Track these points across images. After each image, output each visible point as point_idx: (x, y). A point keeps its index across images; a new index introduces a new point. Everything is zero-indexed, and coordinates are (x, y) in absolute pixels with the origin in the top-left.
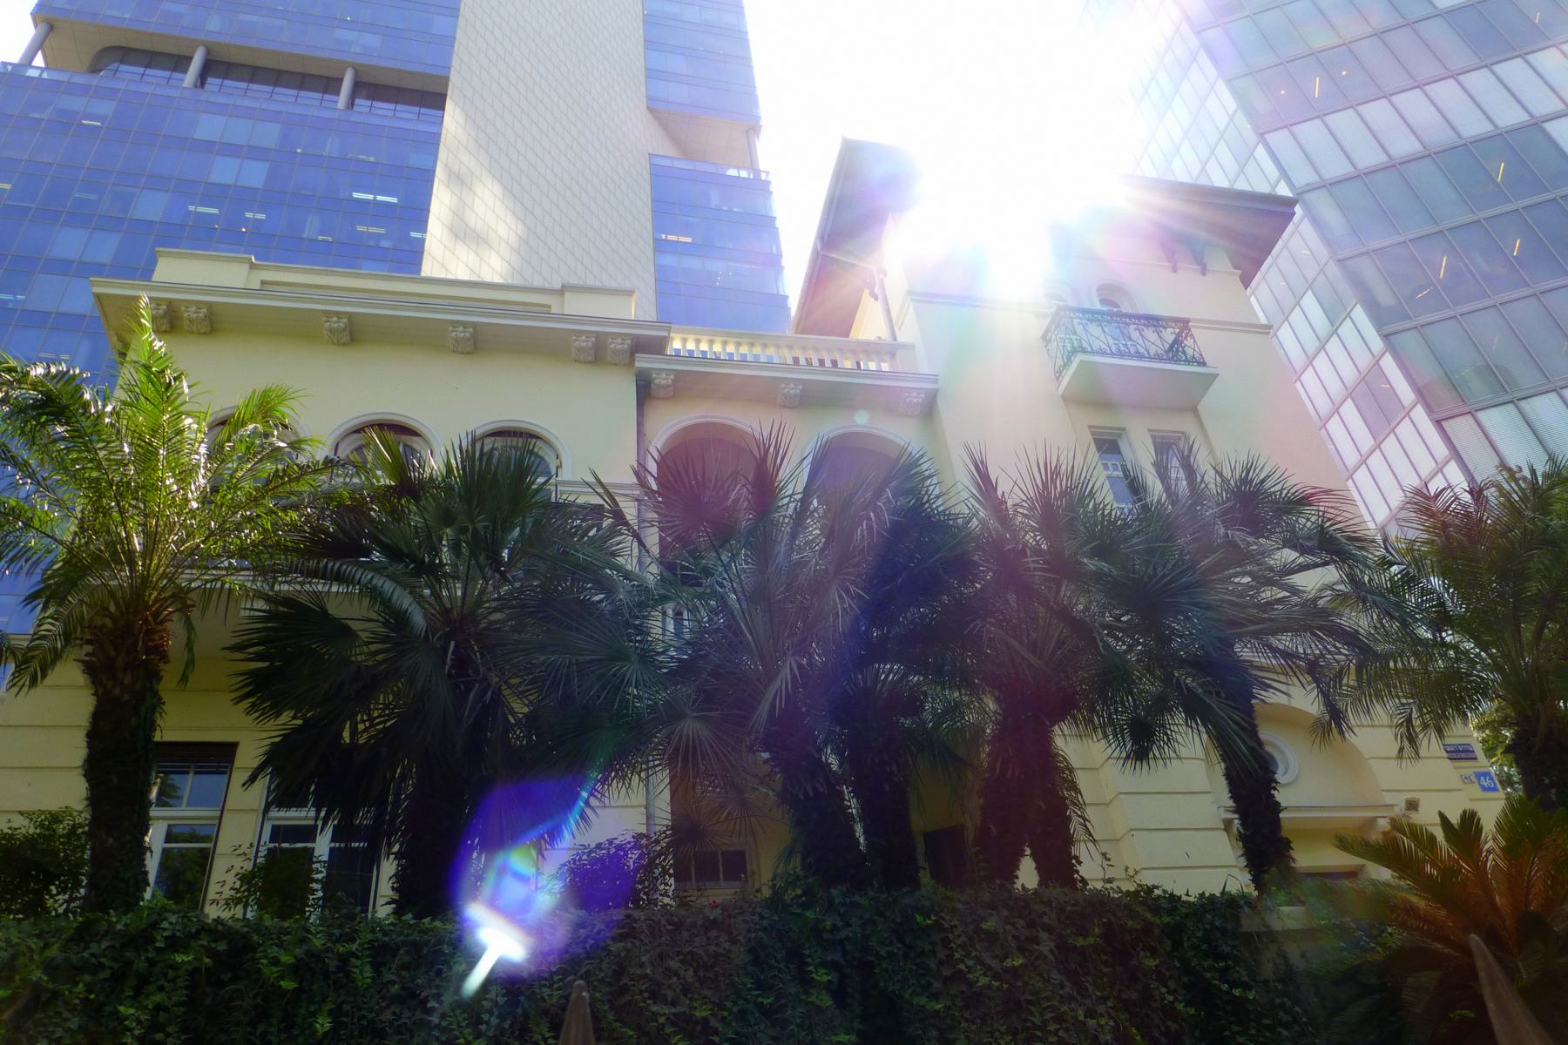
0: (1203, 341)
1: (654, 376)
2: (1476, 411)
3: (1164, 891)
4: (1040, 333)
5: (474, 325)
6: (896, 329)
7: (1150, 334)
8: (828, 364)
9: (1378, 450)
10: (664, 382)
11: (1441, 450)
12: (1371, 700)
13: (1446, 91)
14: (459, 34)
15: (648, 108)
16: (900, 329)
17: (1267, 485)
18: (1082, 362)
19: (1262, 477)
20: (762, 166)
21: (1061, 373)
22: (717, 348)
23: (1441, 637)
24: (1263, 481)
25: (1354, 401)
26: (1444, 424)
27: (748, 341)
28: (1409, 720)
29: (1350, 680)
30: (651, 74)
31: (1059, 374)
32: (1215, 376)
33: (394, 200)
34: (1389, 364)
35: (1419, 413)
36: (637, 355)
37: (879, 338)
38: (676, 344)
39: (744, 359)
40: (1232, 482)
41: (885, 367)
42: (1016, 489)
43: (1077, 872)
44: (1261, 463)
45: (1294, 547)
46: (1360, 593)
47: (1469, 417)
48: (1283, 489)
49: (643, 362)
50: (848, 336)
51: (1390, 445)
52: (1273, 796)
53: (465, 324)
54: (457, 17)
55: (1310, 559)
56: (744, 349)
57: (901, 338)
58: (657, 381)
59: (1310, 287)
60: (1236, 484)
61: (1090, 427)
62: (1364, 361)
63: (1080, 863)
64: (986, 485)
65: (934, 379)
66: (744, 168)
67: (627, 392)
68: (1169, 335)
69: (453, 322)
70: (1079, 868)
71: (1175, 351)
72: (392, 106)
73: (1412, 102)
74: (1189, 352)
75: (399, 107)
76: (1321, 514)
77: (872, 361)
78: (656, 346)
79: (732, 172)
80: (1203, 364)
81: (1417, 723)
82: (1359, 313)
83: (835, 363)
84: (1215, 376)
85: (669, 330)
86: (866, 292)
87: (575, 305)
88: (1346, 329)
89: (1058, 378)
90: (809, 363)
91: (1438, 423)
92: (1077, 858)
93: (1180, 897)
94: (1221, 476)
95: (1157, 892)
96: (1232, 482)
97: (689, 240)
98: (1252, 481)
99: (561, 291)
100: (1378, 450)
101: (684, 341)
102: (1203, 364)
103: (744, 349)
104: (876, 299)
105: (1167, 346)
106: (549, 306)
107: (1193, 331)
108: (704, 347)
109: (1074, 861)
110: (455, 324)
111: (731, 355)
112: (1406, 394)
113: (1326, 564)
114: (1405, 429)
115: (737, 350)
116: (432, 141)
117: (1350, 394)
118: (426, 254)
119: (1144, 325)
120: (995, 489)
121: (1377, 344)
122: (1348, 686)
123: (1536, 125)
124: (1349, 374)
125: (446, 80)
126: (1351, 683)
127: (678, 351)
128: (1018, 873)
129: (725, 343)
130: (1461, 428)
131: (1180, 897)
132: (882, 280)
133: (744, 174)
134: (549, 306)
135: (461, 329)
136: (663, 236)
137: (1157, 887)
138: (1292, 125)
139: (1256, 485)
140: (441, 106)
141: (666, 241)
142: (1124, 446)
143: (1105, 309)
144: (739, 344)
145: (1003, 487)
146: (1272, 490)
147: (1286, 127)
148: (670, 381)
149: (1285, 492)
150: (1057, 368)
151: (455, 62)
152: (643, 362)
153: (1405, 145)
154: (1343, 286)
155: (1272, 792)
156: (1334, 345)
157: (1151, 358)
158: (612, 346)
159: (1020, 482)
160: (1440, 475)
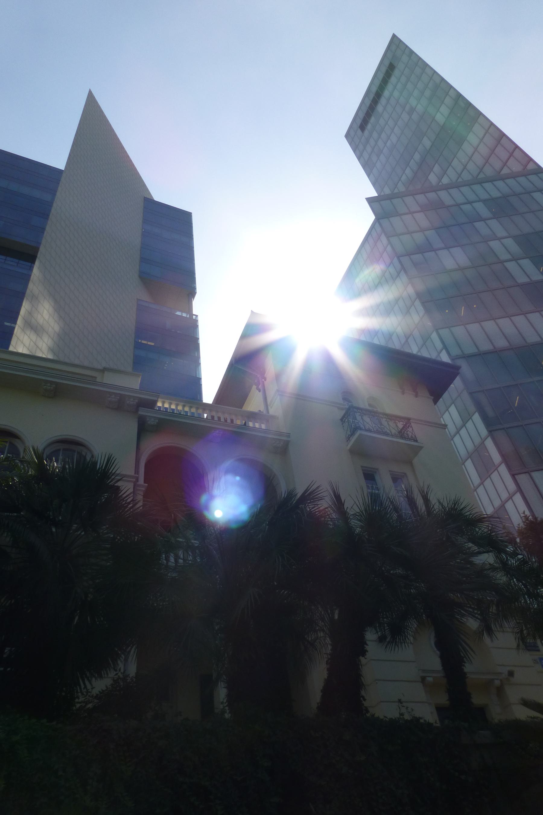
0: (417, 430)
1: (148, 419)
2: (531, 472)
3: (425, 721)
4: (340, 418)
5: (56, 383)
6: (269, 407)
7: (392, 424)
8: (216, 419)
9: (482, 485)
11: (512, 486)
12: (502, 619)
13: (520, 320)
14: (48, 228)
15: (139, 276)
16: (271, 408)
17: (463, 512)
18: (360, 435)
19: (461, 508)
20: (194, 312)
21: (349, 438)
22: (180, 408)
23: (537, 592)
24: (463, 509)
25: (472, 460)
26: (516, 477)
27: (182, 404)
28: (522, 631)
29: (493, 609)
31: (348, 439)
32: (421, 448)
34: (489, 443)
35: (503, 469)
36: (140, 408)
37: (260, 411)
38: (159, 404)
39: (193, 415)
40: (447, 509)
41: (263, 427)
43: (363, 704)
44: (461, 500)
45: (473, 543)
46: (505, 567)
47: (527, 474)
48: (470, 514)
49: (143, 412)
50: (242, 409)
51: (488, 483)
52: (365, 647)
53: (51, 383)
55: (482, 549)
56: (193, 410)
57: (272, 412)
59: (453, 403)
60: (449, 509)
61: (362, 467)
62: (477, 441)
63: (365, 700)
65: (288, 435)
66: (185, 312)
67: (133, 427)
68: (400, 425)
70: (363, 702)
71: (401, 434)
73: (505, 323)
74: (410, 434)
75: (8, 258)
76: (490, 528)
77: (257, 422)
79: (178, 313)
80: (416, 441)
81: (525, 632)
82: (477, 417)
83: (232, 421)
84: (421, 448)
85: (158, 397)
86: (254, 387)
88: (469, 425)
89: (348, 440)
90: (226, 421)
91: (513, 476)
92: (363, 697)
93: (433, 724)
94: (442, 505)
95: (422, 721)
96: (447, 509)
97: (152, 344)
98: (457, 509)
99: (103, 371)
100: (482, 485)
101: (163, 403)
102: (416, 441)
103: (193, 410)
104: (260, 391)
105: (399, 430)
106: (96, 378)
107: (412, 424)
108: (173, 407)
109: (362, 699)
110: (46, 382)
111: (187, 412)
112: (496, 457)
113: (488, 552)
114: (495, 476)
115: (190, 410)
116: (26, 279)
117: (470, 456)
118: (14, 335)
119: (389, 419)
121: (484, 432)
122: (492, 612)
123: (447, 248)
124: (470, 446)
126: (494, 611)
127: (160, 407)
128: (104, 688)
130: (523, 479)
131: (433, 724)
132: (263, 382)
133: (184, 315)
134: (96, 378)
135: (49, 385)
136: (140, 341)
137: (421, 718)
138: (451, 327)
139: (458, 511)
140: (33, 262)
141: (141, 343)
142: (377, 478)
143: (370, 409)
144: (191, 407)
145: (348, 505)
146: (467, 514)
147: (448, 327)
148: (155, 423)
149: (471, 516)
150: (347, 436)
151: (43, 242)
152: (143, 412)
153: (501, 343)
154: (472, 408)
155: (463, 667)
156: (463, 432)
157: (392, 435)
158: (128, 402)
160: (482, 485)
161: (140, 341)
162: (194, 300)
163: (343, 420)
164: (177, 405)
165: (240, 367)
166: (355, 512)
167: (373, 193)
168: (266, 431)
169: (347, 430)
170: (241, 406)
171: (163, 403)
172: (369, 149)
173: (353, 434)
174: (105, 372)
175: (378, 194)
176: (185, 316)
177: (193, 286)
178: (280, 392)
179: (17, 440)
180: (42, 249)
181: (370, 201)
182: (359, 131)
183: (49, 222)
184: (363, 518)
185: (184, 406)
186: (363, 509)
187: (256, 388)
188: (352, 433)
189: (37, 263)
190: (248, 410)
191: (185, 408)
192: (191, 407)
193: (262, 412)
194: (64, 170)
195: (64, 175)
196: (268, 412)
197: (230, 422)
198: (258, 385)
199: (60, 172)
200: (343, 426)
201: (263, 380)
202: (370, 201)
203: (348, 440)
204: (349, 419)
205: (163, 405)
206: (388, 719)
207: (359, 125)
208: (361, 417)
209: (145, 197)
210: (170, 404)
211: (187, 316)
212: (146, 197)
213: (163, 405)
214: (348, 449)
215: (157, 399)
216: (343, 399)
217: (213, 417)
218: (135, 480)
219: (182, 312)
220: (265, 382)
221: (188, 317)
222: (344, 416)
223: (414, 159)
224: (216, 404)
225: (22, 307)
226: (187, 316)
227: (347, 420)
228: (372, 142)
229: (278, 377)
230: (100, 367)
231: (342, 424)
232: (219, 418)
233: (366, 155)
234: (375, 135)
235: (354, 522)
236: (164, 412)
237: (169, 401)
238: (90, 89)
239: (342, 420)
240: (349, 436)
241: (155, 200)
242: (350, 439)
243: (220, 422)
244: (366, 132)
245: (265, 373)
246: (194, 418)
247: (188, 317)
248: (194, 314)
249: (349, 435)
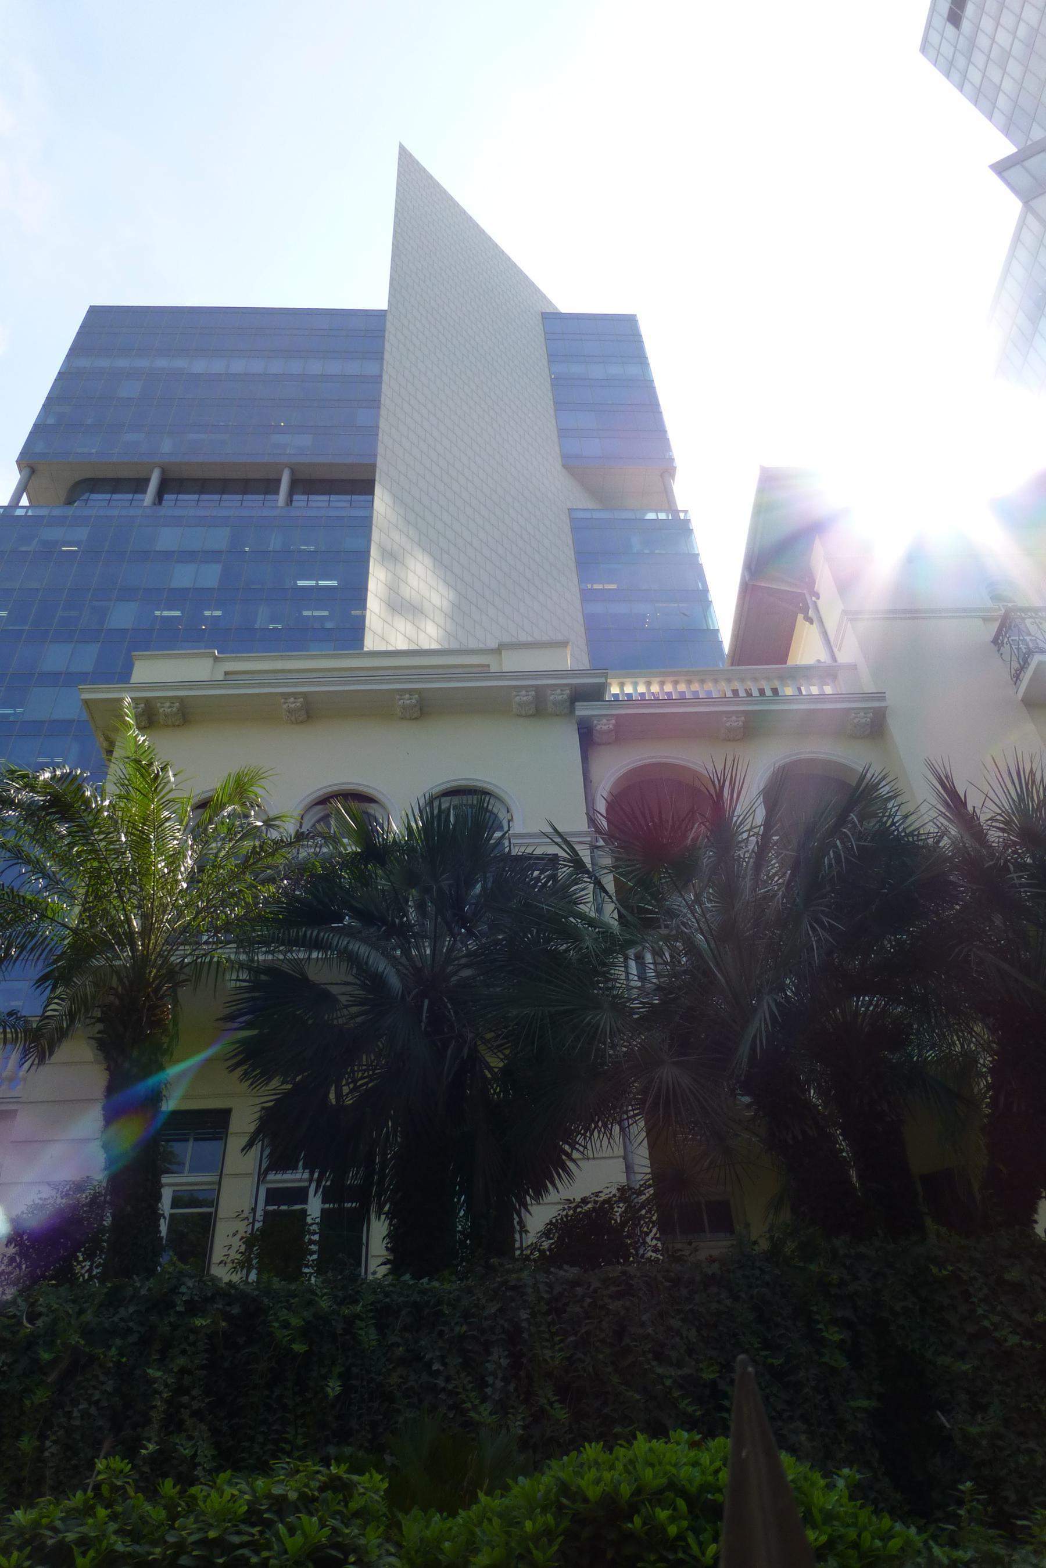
1: (595, 722)
6: (835, 650)
10: (605, 728)
14: (382, 424)
15: (563, 466)
16: (839, 650)
20: (680, 506)
22: (655, 688)
27: (658, 679)
30: (563, 433)
33: (335, 583)
36: (577, 704)
37: (819, 661)
38: (615, 690)
42: (989, 803)
53: (411, 692)
54: (379, 408)
58: (598, 727)
64: (955, 802)
65: (880, 696)
66: (661, 511)
69: (398, 691)
72: (326, 498)
75: (333, 497)
78: (595, 693)
79: (651, 516)
83: (775, 691)
87: (513, 662)
97: (614, 586)
99: (498, 651)
101: (622, 685)
104: (811, 622)
111: (669, 694)
115: (675, 688)
116: (365, 525)
120: (965, 804)
125: (373, 467)
129: (662, 684)
132: (815, 603)
133: (662, 516)
134: (488, 666)
136: (589, 586)
144: (676, 683)
145: (973, 802)
150: (1013, 672)
151: (381, 449)
152: (583, 710)
158: (552, 697)
159: (992, 795)
161: (589, 586)
162: (676, 479)
163: (999, 641)
164: (648, 684)
165: (763, 585)
166: (994, 815)
167: (1007, 148)
168: (838, 697)
169: (1011, 661)
170: (783, 659)
171: (622, 685)
172: (979, 59)
173: (1023, 668)
174: (504, 652)
175: (1017, 148)
176: (665, 518)
177: (667, 457)
178: (851, 616)
179: (373, 805)
180: (380, 463)
181: (1001, 168)
182: (950, 28)
183: (383, 412)
184: (1016, 825)
185: (662, 684)
186: (1007, 808)
187: (804, 618)
188: (1022, 663)
189: (378, 490)
190: (798, 663)
191: (625, 689)
192: (676, 683)
193: (825, 662)
194: (386, 309)
195: (389, 317)
196: (835, 659)
197: (758, 695)
198: (805, 610)
199: (379, 316)
200: (1001, 654)
201: (814, 598)
202: (1001, 168)
203: (1017, 680)
204: (1010, 637)
205: (622, 689)
206: (649, 1174)
207: (946, 15)
208: (1037, 625)
209: (542, 313)
210: (648, 684)
211: (668, 516)
212: (544, 311)
213: (622, 689)
214: (1020, 699)
215: (603, 680)
216: (992, 598)
217: (735, 692)
218: (589, 839)
219: (657, 512)
220: (818, 601)
221: (670, 518)
222: (999, 633)
223: (998, 44)
224: (732, 665)
225: (370, 576)
226: (668, 516)
227: (1006, 640)
228: (983, 41)
229: (844, 587)
230: (493, 644)
231: (999, 651)
232: (762, 692)
233: (975, 76)
234: (987, 24)
235: (995, 837)
236: (652, 702)
237: (643, 680)
238: (400, 144)
239: (995, 641)
240: (1018, 672)
241: (563, 311)
242: (1021, 677)
243: (765, 698)
244: (966, 25)
245: (814, 583)
246: (713, 700)
247: (670, 518)
248: (679, 509)
249: (1016, 671)
